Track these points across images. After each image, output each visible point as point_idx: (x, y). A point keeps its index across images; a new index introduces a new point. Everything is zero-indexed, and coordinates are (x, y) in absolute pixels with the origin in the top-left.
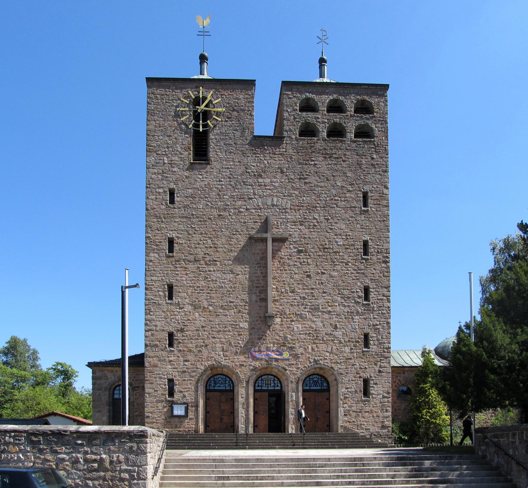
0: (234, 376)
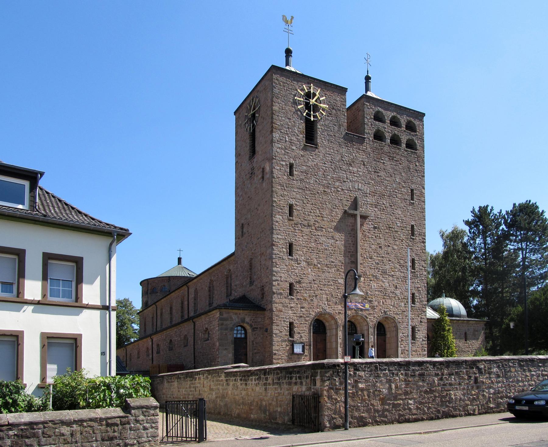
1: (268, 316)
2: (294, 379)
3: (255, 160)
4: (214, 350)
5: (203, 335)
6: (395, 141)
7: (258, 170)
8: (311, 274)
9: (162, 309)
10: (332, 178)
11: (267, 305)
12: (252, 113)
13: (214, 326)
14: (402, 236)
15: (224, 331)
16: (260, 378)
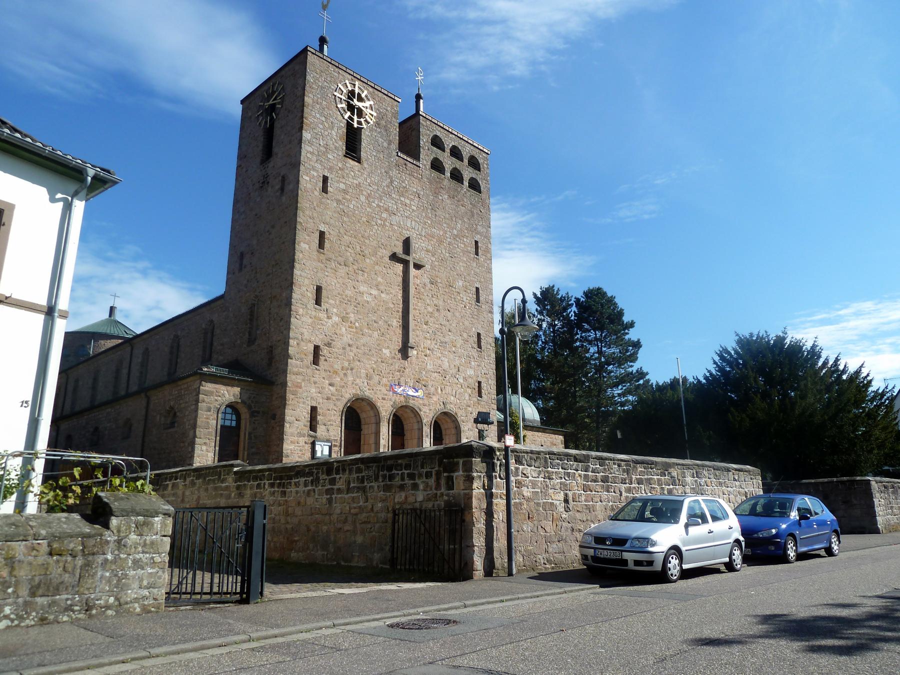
0: (291, 187)
1: (278, 394)
2: (398, 478)
3: (271, 165)
4: (182, 445)
5: (163, 419)
6: (456, 176)
7: (275, 178)
9: (77, 381)
10: (378, 206)
11: (277, 375)
12: (271, 102)
13: (186, 402)
14: (465, 300)
16: (315, 482)
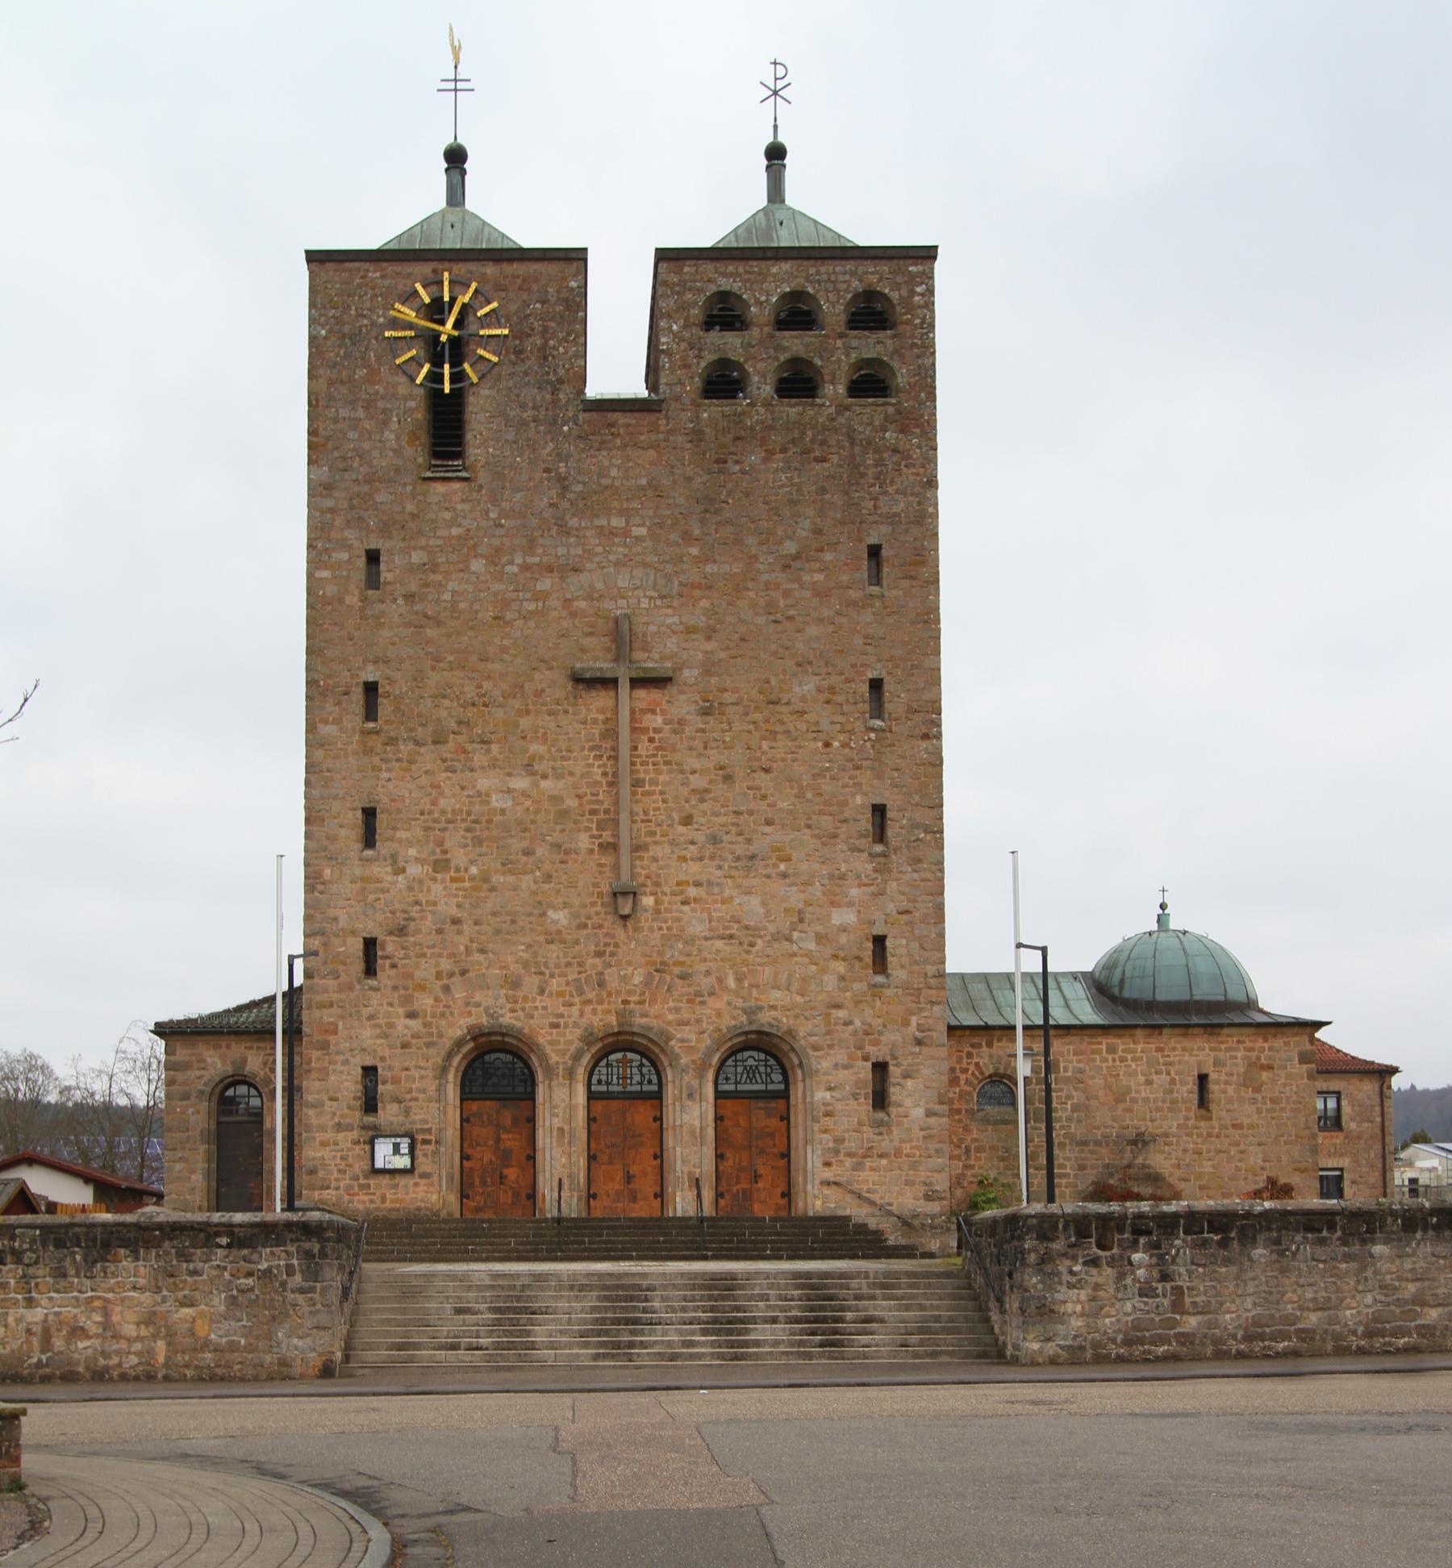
8: (443, 897)
15: (179, 1103)
